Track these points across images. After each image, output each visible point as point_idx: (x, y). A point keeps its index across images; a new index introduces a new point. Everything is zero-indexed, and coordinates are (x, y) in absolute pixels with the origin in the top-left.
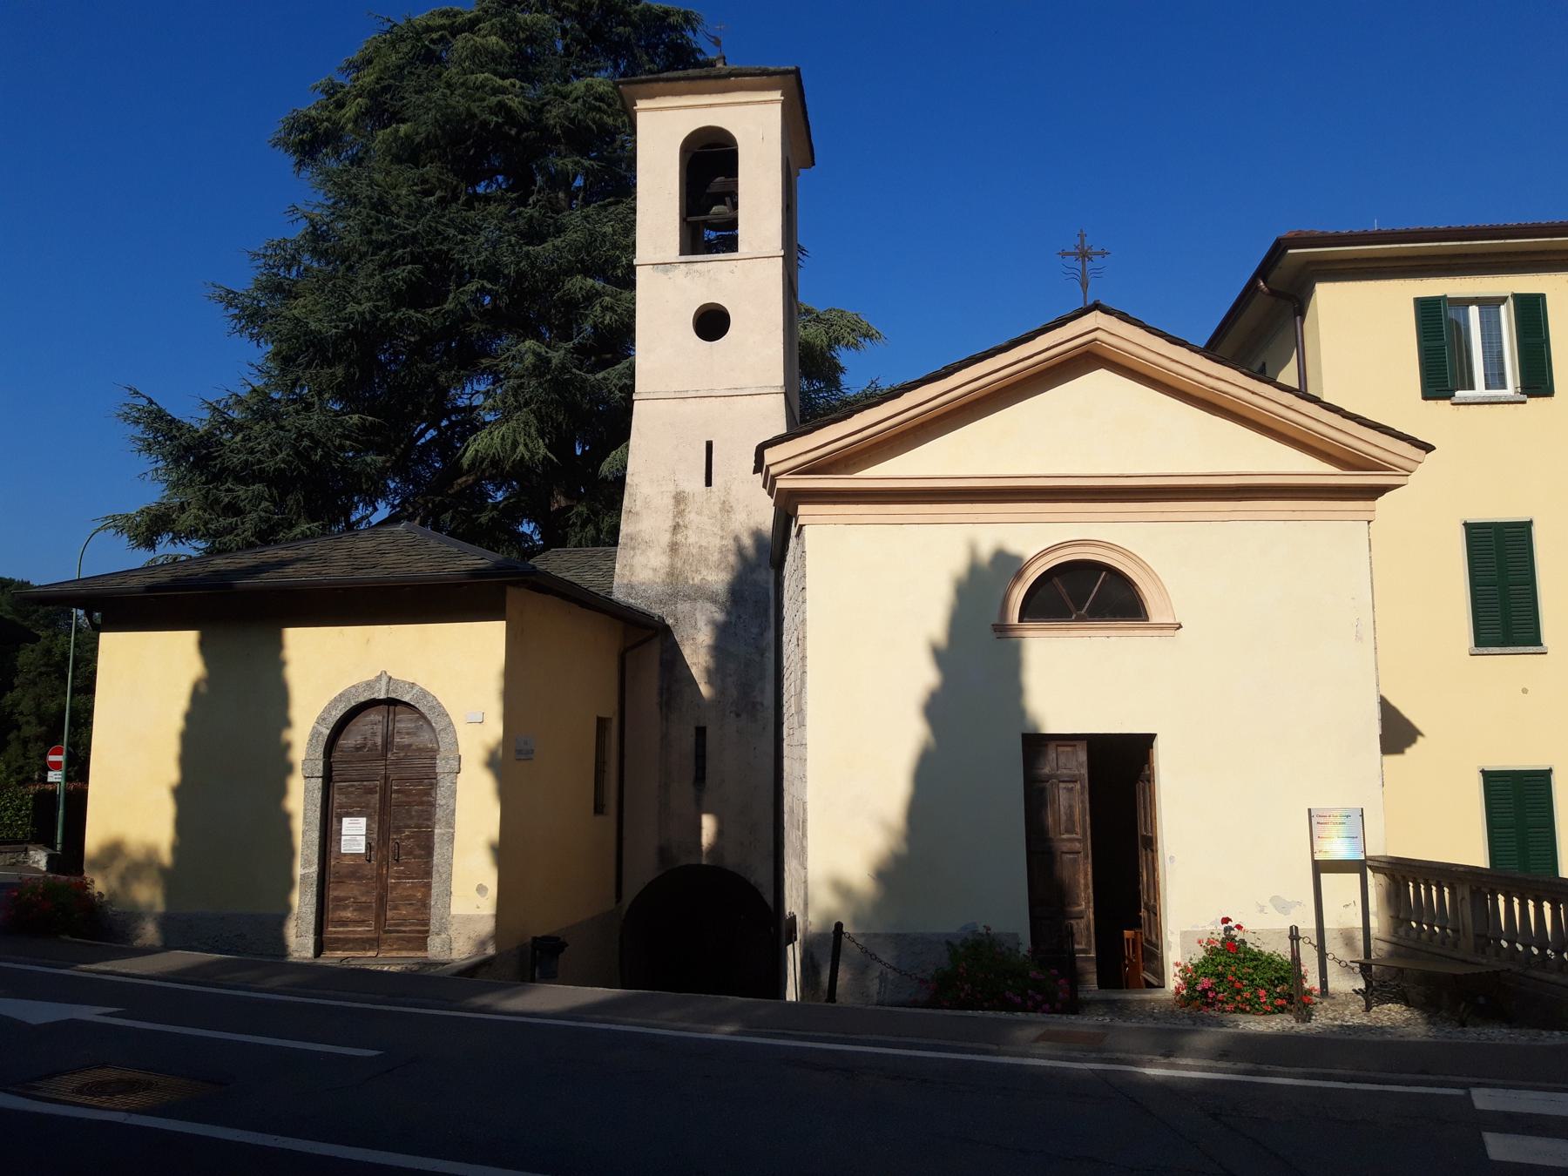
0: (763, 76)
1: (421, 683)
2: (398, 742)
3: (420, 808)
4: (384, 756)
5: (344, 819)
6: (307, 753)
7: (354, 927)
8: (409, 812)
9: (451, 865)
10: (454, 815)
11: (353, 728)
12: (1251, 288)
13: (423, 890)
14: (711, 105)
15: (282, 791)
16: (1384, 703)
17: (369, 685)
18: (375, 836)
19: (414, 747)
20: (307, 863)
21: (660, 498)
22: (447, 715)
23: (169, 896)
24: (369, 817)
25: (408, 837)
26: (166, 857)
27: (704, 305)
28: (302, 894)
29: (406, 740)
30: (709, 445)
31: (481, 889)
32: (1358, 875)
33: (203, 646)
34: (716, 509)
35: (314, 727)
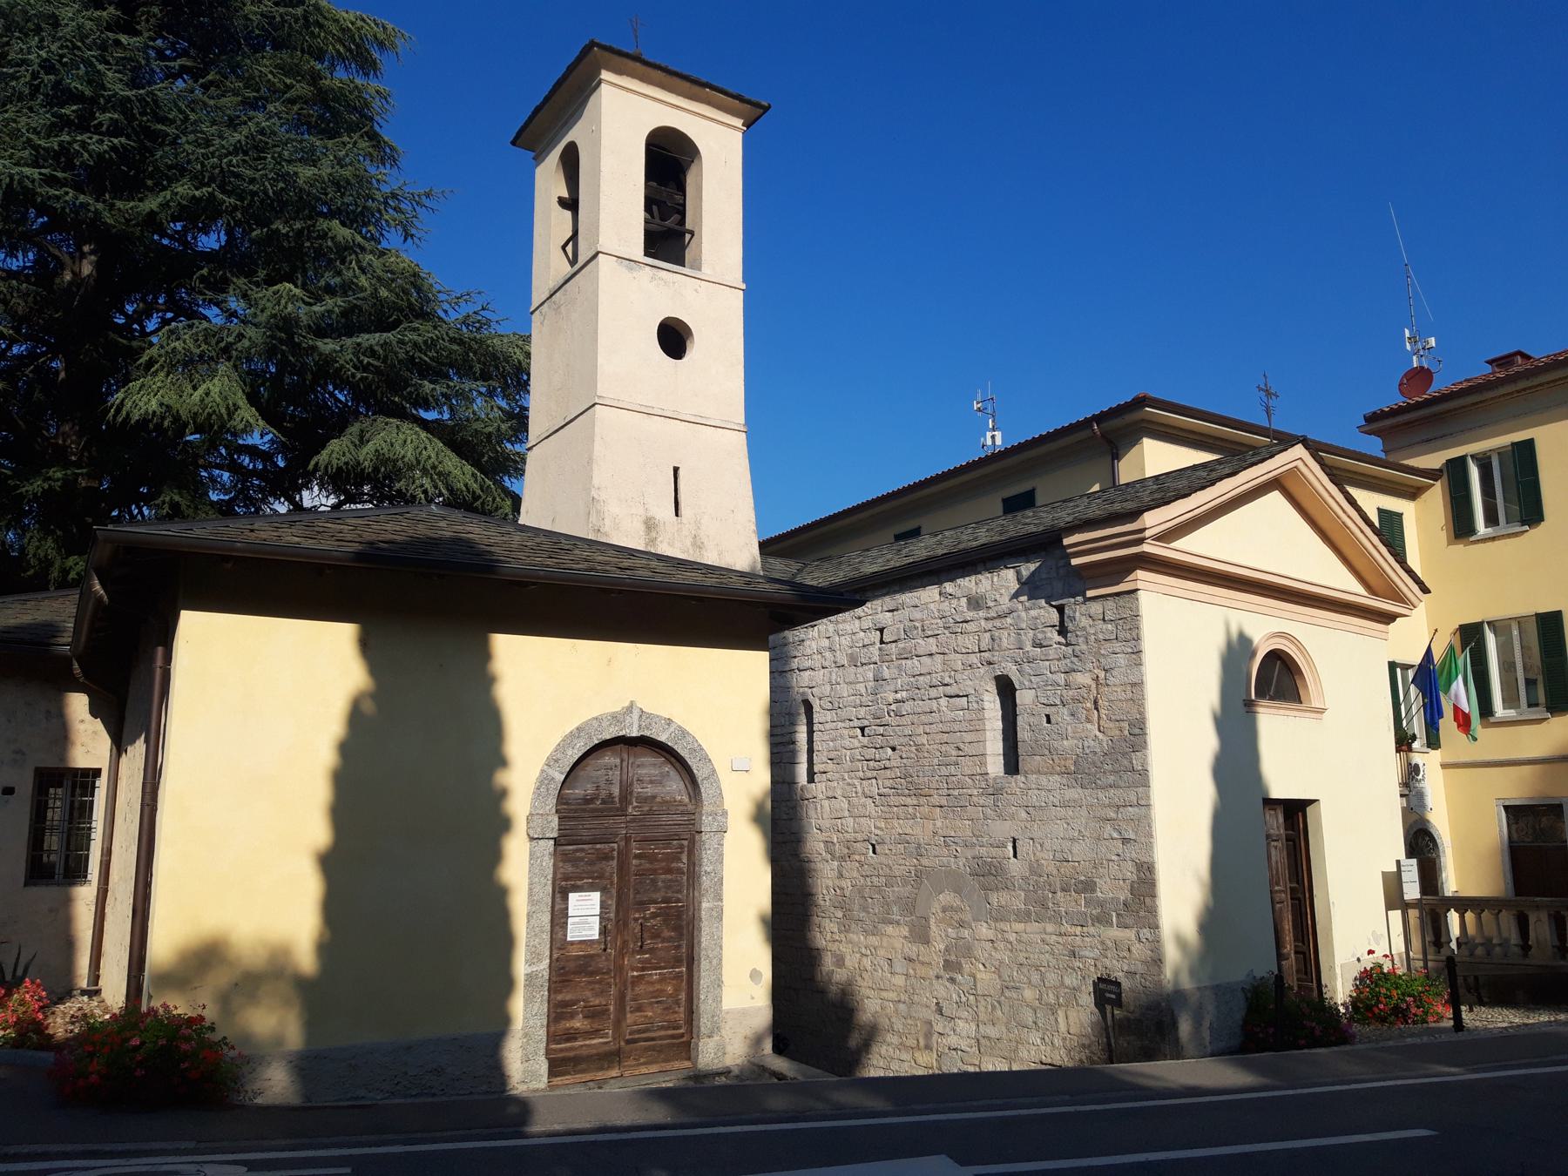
0: (737, 99)
1: (678, 720)
2: (639, 793)
3: (669, 877)
4: (622, 811)
5: (571, 895)
6: (533, 806)
7: (585, 1039)
8: (654, 882)
11: (582, 773)
12: (1087, 423)
13: (674, 982)
14: (678, 107)
15: (495, 856)
17: (615, 718)
18: (612, 915)
19: (658, 799)
20: (533, 958)
21: (630, 521)
22: (710, 760)
23: (311, 1025)
24: (603, 890)
25: (654, 915)
26: (306, 959)
28: (529, 1001)
29: (649, 790)
30: (676, 470)
31: (755, 975)
32: (1400, 911)
33: (366, 646)
34: (688, 542)
35: (543, 771)
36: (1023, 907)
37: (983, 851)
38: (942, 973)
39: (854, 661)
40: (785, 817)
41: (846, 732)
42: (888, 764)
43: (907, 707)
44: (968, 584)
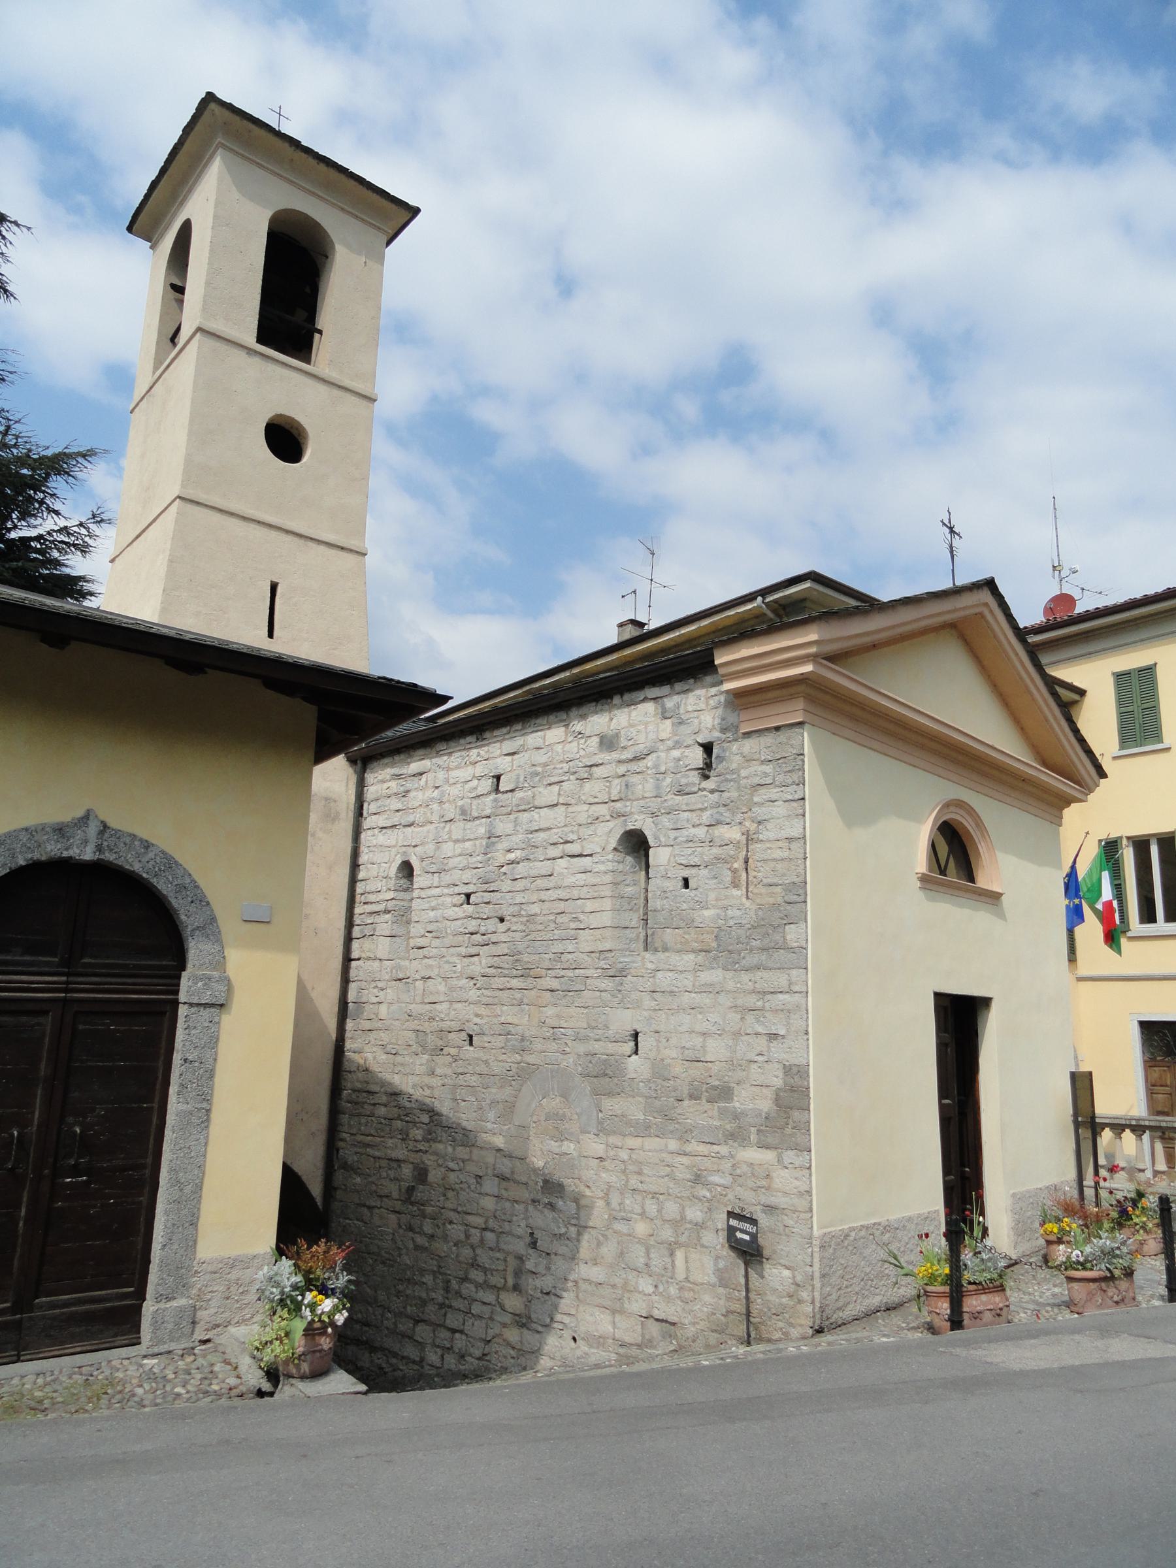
9: (201, 1167)
10: (212, 1077)
16: (1121, 956)
22: (208, 903)
27: (281, 415)
30: (274, 588)
36: (642, 1117)
37: (597, 1047)
38: (540, 1196)
39: (466, 815)
40: (375, 1000)
41: (448, 900)
42: (494, 938)
43: (521, 870)
44: (598, 722)
